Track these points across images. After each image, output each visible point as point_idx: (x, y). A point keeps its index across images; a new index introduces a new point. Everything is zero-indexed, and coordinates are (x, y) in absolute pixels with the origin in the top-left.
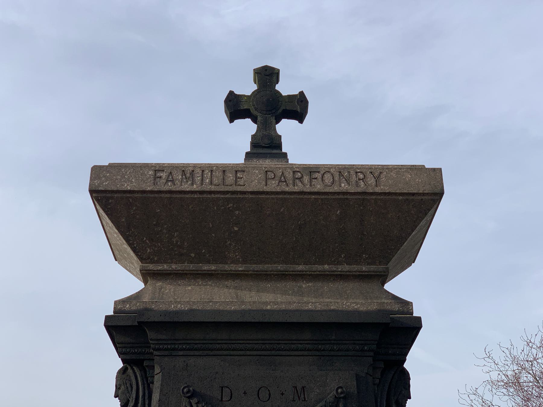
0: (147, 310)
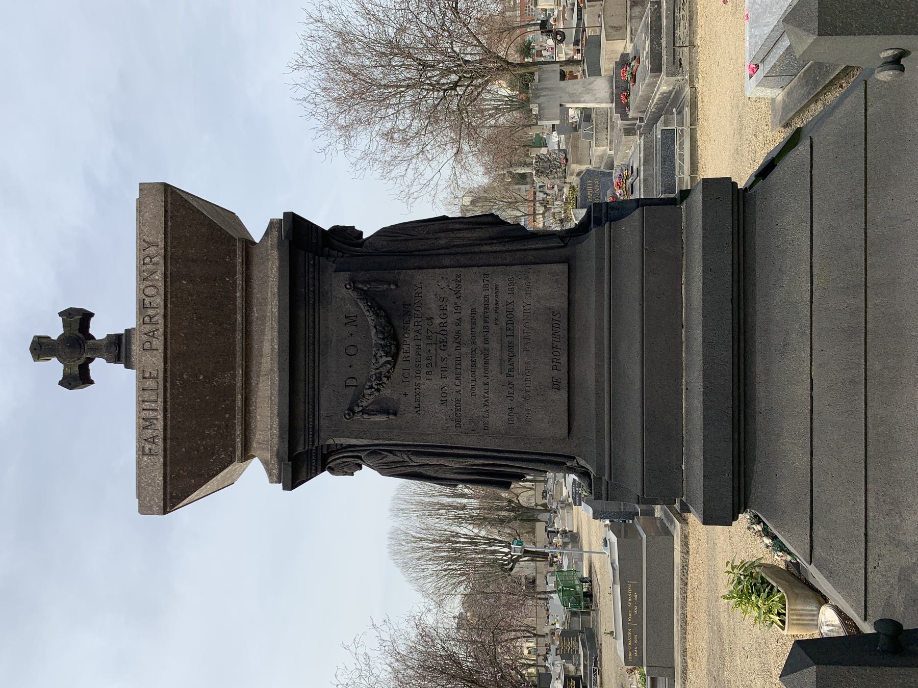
0: (278, 455)
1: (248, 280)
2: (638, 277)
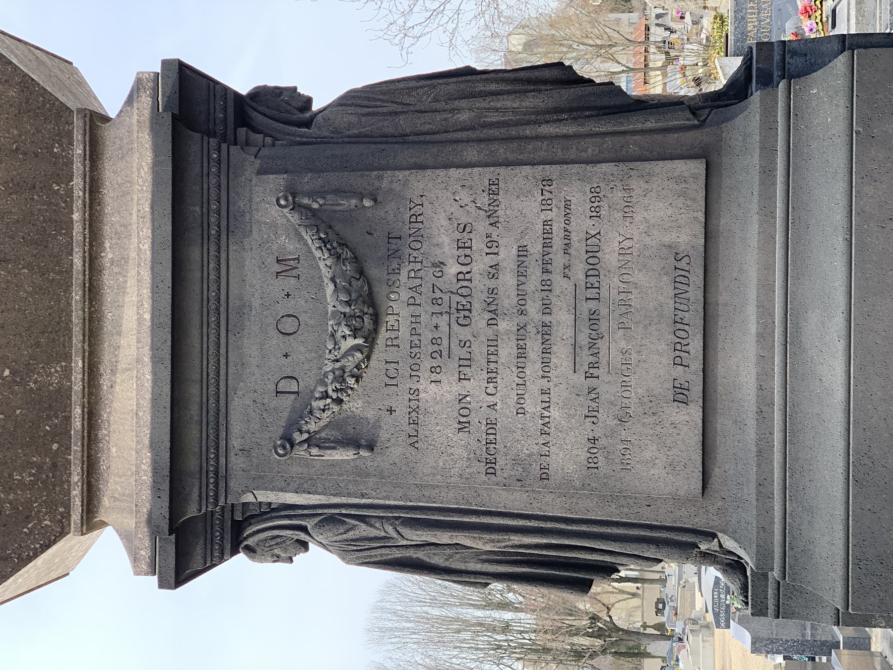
0: (149, 521)
1: (94, 187)
2: (841, 186)
